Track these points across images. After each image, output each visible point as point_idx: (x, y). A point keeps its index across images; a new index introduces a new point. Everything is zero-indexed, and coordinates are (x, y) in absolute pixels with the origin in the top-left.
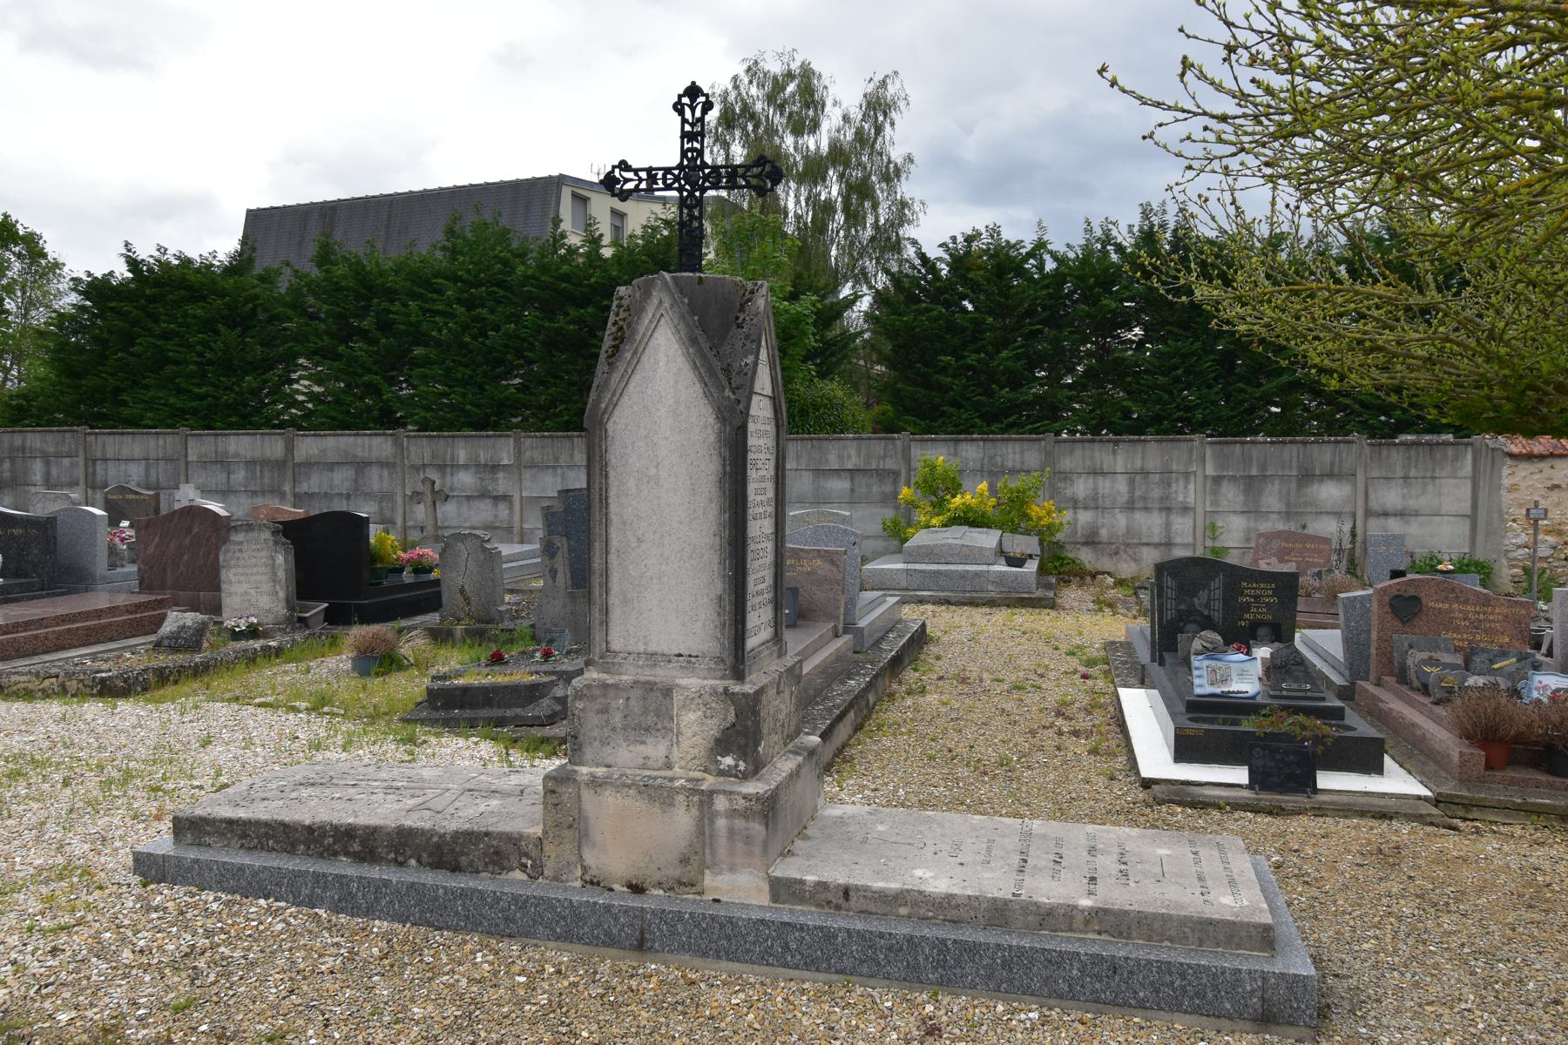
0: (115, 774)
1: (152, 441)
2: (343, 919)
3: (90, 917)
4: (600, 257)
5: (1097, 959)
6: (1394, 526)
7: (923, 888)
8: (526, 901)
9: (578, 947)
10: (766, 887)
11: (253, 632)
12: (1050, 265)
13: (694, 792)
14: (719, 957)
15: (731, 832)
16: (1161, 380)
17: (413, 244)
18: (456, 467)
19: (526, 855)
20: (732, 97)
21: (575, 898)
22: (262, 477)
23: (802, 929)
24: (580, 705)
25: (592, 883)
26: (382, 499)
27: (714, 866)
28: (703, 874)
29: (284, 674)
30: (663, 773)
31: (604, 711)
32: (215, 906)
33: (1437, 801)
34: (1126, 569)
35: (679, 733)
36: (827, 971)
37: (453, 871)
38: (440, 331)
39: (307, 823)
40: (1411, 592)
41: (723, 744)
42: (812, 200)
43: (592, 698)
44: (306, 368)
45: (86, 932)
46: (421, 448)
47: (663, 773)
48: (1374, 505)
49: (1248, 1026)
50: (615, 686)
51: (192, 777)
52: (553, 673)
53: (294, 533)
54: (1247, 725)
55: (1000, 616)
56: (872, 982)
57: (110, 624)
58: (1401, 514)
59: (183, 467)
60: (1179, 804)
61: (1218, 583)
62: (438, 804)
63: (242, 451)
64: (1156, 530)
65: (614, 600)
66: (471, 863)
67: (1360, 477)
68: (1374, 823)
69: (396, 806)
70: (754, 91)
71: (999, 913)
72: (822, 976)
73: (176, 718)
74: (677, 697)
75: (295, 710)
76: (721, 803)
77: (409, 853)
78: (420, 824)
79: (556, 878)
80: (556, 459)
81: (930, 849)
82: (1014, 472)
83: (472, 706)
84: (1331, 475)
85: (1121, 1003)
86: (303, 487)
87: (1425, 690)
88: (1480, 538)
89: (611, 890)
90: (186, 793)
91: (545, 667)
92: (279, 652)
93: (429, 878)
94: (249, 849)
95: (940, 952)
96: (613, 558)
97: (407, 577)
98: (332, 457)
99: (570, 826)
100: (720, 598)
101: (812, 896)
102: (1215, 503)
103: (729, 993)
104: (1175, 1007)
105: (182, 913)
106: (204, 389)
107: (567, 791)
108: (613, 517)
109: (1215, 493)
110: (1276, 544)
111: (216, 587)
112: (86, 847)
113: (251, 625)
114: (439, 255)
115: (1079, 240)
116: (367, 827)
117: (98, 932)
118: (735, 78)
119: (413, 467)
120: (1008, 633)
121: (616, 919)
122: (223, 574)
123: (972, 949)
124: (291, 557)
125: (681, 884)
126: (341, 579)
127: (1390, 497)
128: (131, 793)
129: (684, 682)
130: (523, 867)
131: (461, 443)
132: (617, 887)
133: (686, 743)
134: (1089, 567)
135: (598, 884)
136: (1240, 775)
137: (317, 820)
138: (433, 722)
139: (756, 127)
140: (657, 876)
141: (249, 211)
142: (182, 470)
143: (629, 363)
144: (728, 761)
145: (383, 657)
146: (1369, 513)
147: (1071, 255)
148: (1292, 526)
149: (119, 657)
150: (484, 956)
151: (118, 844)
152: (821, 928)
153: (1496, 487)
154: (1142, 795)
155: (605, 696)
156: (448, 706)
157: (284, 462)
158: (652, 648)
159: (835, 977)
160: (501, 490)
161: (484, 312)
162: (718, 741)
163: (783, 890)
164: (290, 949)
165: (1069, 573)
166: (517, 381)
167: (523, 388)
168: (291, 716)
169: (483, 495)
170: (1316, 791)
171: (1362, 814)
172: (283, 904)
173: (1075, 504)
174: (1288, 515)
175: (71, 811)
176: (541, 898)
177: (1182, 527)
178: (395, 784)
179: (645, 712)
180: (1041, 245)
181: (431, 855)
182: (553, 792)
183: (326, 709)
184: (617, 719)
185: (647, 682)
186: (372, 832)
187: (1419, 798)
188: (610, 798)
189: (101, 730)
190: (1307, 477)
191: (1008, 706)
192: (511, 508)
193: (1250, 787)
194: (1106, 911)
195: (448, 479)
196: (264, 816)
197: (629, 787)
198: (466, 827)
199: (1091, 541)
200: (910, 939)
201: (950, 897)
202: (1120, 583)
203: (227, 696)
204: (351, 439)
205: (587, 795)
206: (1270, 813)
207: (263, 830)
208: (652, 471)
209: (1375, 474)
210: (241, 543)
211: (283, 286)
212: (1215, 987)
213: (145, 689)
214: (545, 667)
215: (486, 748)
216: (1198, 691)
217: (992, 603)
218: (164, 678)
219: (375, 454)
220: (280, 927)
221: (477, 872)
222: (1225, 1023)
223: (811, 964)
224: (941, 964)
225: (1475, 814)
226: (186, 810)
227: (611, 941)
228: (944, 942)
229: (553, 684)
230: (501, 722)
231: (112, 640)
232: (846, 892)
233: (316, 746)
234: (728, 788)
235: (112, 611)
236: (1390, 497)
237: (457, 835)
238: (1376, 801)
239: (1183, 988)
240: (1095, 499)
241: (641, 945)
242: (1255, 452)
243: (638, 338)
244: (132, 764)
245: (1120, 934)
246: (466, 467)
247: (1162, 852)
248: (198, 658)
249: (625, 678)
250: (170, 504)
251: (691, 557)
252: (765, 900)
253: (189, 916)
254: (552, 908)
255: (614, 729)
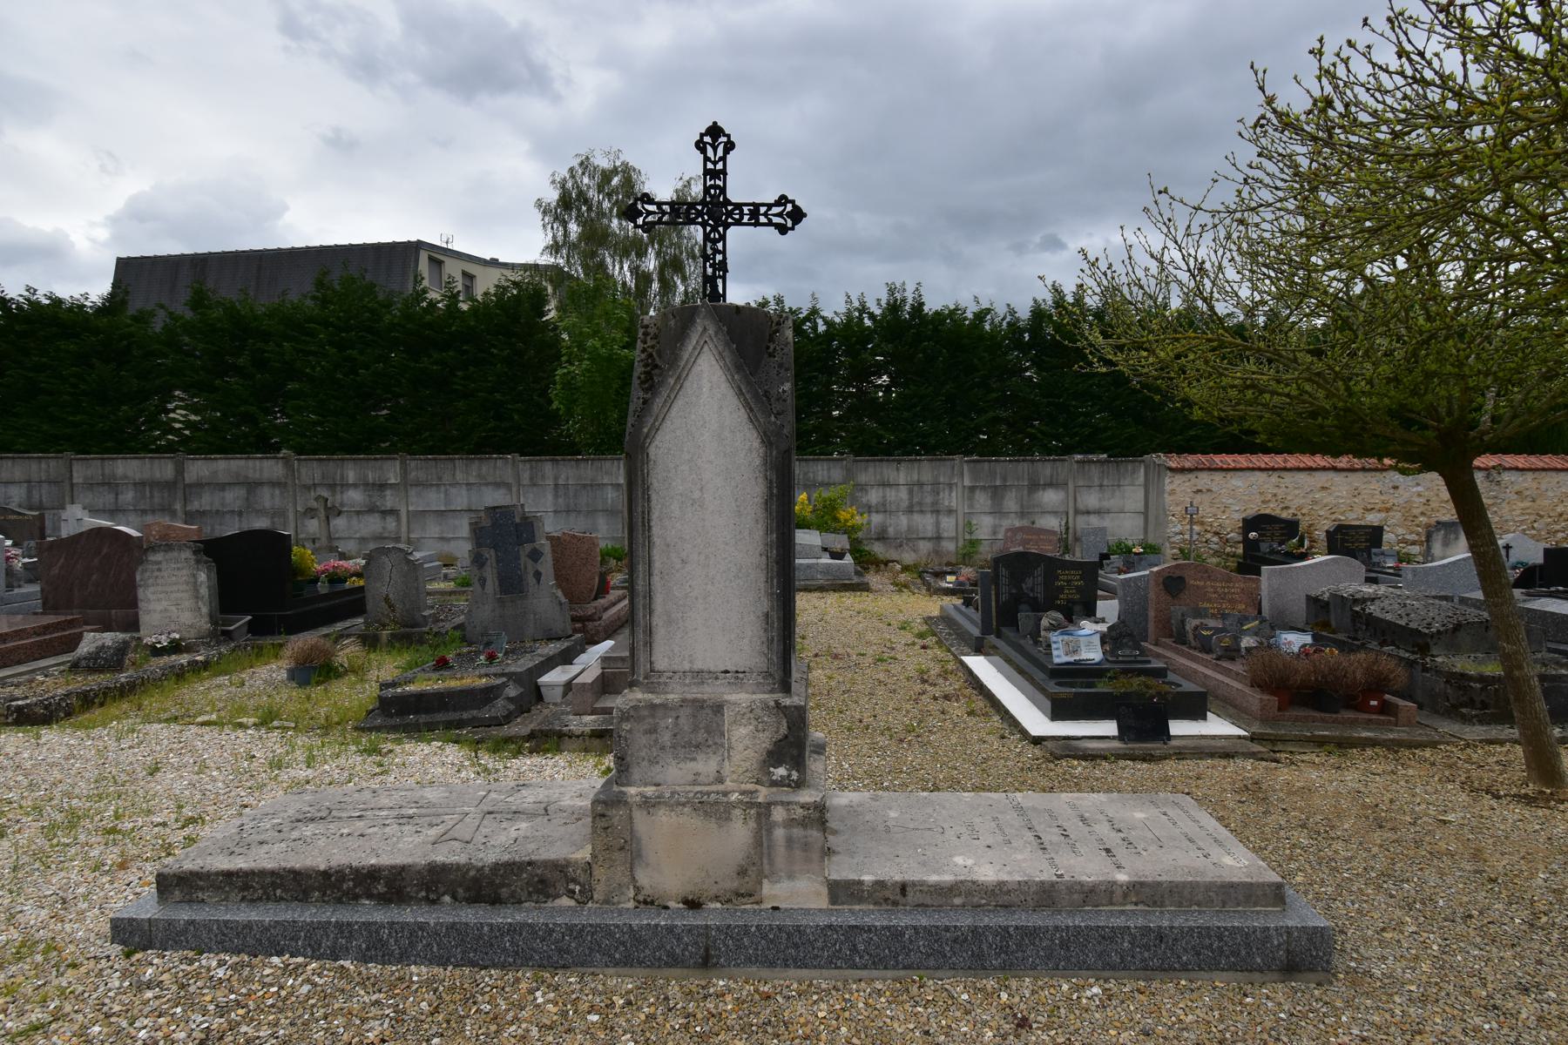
0: (59, 817)
1: (34, 466)
2: (374, 969)
3: (68, 1008)
4: (459, 310)
5: (1146, 931)
6: (1094, 521)
7: (975, 878)
8: (582, 930)
9: (641, 972)
10: (825, 891)
11: (175, 647)
12: (822, 328)
13: (751, 805)
14: (787, 966)
15: (790, 841)
16: (906, 414)
17: (284, 293)
18: (345, 486)
19: (574, 881)
20: (569, 185)
21: (635, 922)
22: (152, 497)
23: (870, 930)
24: (626, 726)
25: (645, 902)
26: (274, 515)
27: (773, 876)
28: (761, 883)
29: (216, 690)
30: (714, 788)
31: (653, 730)
32: (220, 973)
33: (1252, 739)
34: (909, 557)
35: (730, 748)
36: (894, 968)
37: (493, 903)
38: (313, 368)
39: (322, 867)
40: (1178, 573)
41: (775, 755)
42: (635, 270)
43: (640, 719)
44: (182, 400)
45: (67, 1029)
46: (311, 470)
47: (714, 788)
48: (1081, 506)
49: (1276, 976)
50: (664, 706)
51: (149, 812)
52: (503, 675)
53: (214, 551)
54: (1102, 687)
55: (832, 598)
56: (939, 974)
57: (18, 647)
58: (1098, 512)
59: (68, 488)
60: (1074, 757)
61: (1040, 571)
62: (464, 831)
63: (130, 474)
64: (929, 528)
65: (658, 620)
66: (513, 894)
67: (1071, 486)
68: (1223, 762)
69: (418, 839)
70: (586, 180)
71: (1046, 895)
72: (890, 973)
73: (112, 744)
74: (728, 714)
75: (241, 726)
76: (778, 814)
77: (442, 890)
78: (453, 859)
79: (607, 902)
80: (440, 479)
81: (950, 834)
82: (828, 485)
83: (427, 711)
84: (1051, 485)
85: (1167, 969)
86: (195, 505)
87: (1207, 650)
88: (1151, 527)
89: (666, 908)
90: (148, 833)
91: (492, 670)
92: (206, 665)
93: (470, 915)
94: (252, 901)
95: (1003, 938)
96: (656, 579)
97: (323, 588)
98: (222, 478)
99: (622, 849)
100: (767, 615)
101: (870, 894)
102: (971, 506)
103: (815, 1004)
104: (1213, 966)
105: (183, 987)
106: (78, 418)
107: (617, 815)
108: (655, 539)
109: (971, 499)
110: (1019, 537)
111: (133, 603)
112: (44, 913)
113: (173, 641)
114: (309, 302)
115: (842, 309)
116: (393, 867)
117: (84, 1027)
118: (571, 170)
119: (305, 486)
120: (846, 614)
121: (679, 939)
122: (141, 593)
123: (1032, 933)
124: (214, 575)
125: (739, 895)
126: (264, 594)
127: (1091, 500)
128: (82, 838)
129: (733, 697)
130: (571, 894)
131: (350, 465)
132: (672, 904)
133: (737, 757)
134: (881, 557)
135: (652, 903)
136: (1109, 728)
137: (334, 863)
138: (394, 729)
139: (590, 209)
140: (714, 890)
141: (119, 260)
142: (67, 492)
143: (672, 389)
144: (781, 771)
145: (322, 667)
146: (1077, 512)
147: (837, 320)
148: (1025, 523)
149: (31, 681)
150: (544, 994)
151: (83, 905)
152: (888, 928)
153: (1161, 492)
154: (1037, 751)
155: (653, 716)
156: (402, 712)
157: (175, 483)
158: (698, 666)
159: (902, 973)
160: (389, 505)
161: (354, 353)
162: (770, 753)
163: (841, 892)
164: (325, 1018)
165: (868, 562)
166: (385, 412)
167: (388, 418)
168: (240, 733)
169: (372, 510)
170: (1169, 737)
171: (1212, 755)
172: (300, 960)
173: (869, 509)
174: (1022, 514)
175: (15, 869)
176: (599, 926)
177: (948, 525)
178: (404, 812)
179: (695, 729)
180: (814, 312)
181: (468, 889)
182: (603, 816)
183: (276, 723)
184: (666, 738)
185: (695, 701)
186: (400, 872)
187: (1239, 737)
188: (663, 817)
189: (28, 764)
190: (1034, 486)
191: (881, 676)
192: (398, 520)
193: (1121, 737)
194: (1142, 884)
195: (338, 497)
196: (270, 865)
197: (684, 805)
198: (506, 857)
199: (882, 537)
200: (974, 930)
201: (1001, 884)
202: (906, 569)
203: (164, 716)
204: (242, 462)
205: (639, 816)
206: (1144, 760)
207: (268, 880)
208: (697, 495)
209: (1081, 483)
210: (159, 563)
211: (158, 325)
212: (1248, 945)
213: (68, 715)
214: (492, 670)
215: (453, 753)
216: (1057, 660)
217: (821, 589)
218: (88, 701)
219: (266, 476)
220: (305, 989)
221: (520, 902)
222: (1257, 975)
223: (879, 963)
224: (1003, 950)
225: (1279, 747)
226: (171, 864)
227: (674, 961)
228: (1006, 929)
229: (504, 685)
230: (460, 724)
231: (19, 663)
232: (903, 888)
233: (277, 764)
234: (785, 799)
235: (19, 634)
236: (1091, 500)
237: (496, 867)
238: (1213, 743)
239: (1220, 948)
240: (884, 505)
241: (706, 962)
242: (999, 468)
243: (682, 364)
244: (75, 801)
245: (1155, 903)
246: (355, 486)
247: (1139, 815)
248: (123, 678)
249: (671, 696)
250: (57, 528)
251: (736, 577)
252: (823, 902)
253: (192, 989)
254: (611, 934)
255: (663, 748)
